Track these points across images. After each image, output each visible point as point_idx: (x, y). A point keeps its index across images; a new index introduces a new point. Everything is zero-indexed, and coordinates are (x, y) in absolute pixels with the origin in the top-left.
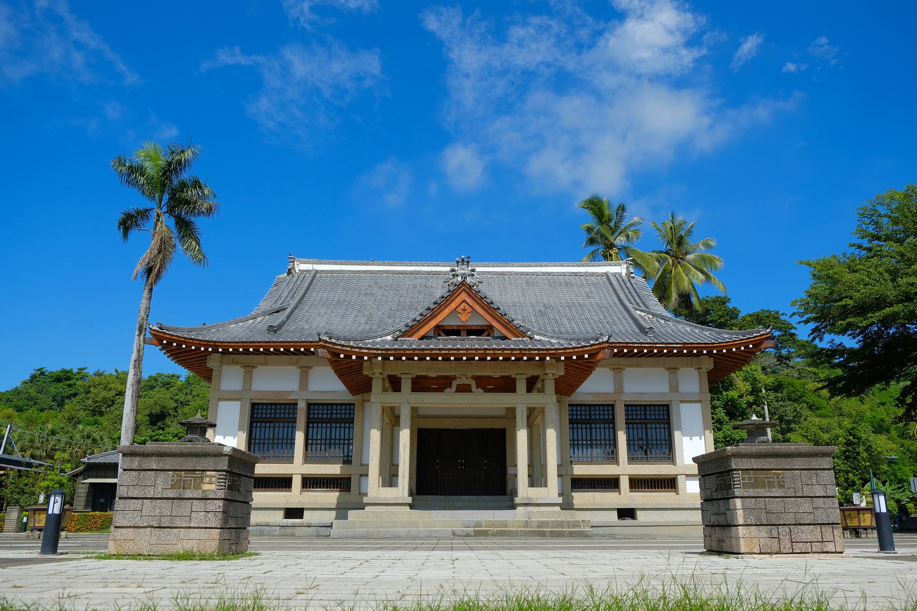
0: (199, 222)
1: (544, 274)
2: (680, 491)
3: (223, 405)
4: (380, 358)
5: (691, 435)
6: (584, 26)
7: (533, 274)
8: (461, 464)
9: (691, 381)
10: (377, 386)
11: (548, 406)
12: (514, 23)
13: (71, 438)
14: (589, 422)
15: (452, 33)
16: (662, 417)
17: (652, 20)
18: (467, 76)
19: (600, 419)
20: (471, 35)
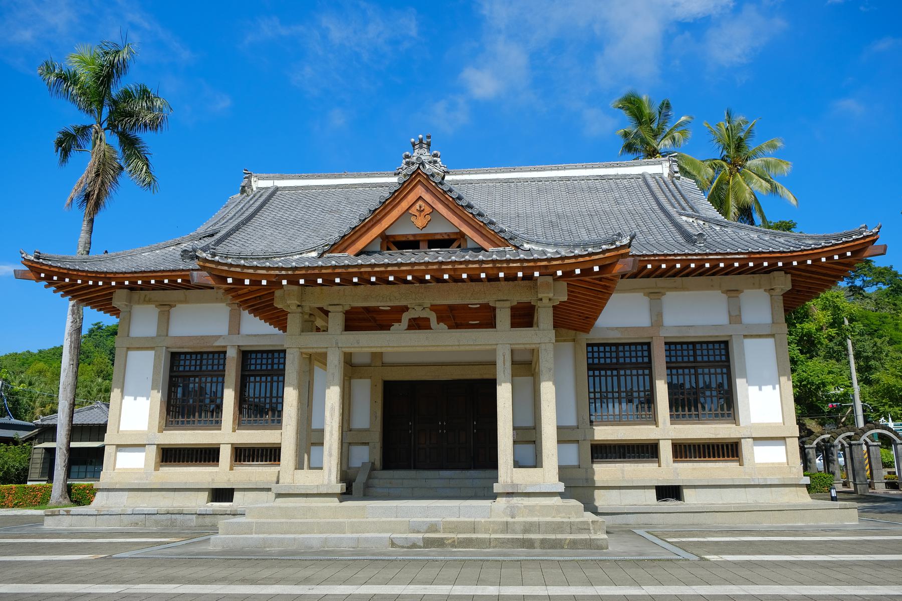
0: (145, 137)
1: (561, 179)
2: (746, 461)
3: (133, 355)
5: (760, 384)
7: (547, 179)
8: (442, 423)
9: (759, 306)
11: (543, 346)
13: (89, 392)
14: (615, 367)
16: (718, 358)
19: (631, 363)
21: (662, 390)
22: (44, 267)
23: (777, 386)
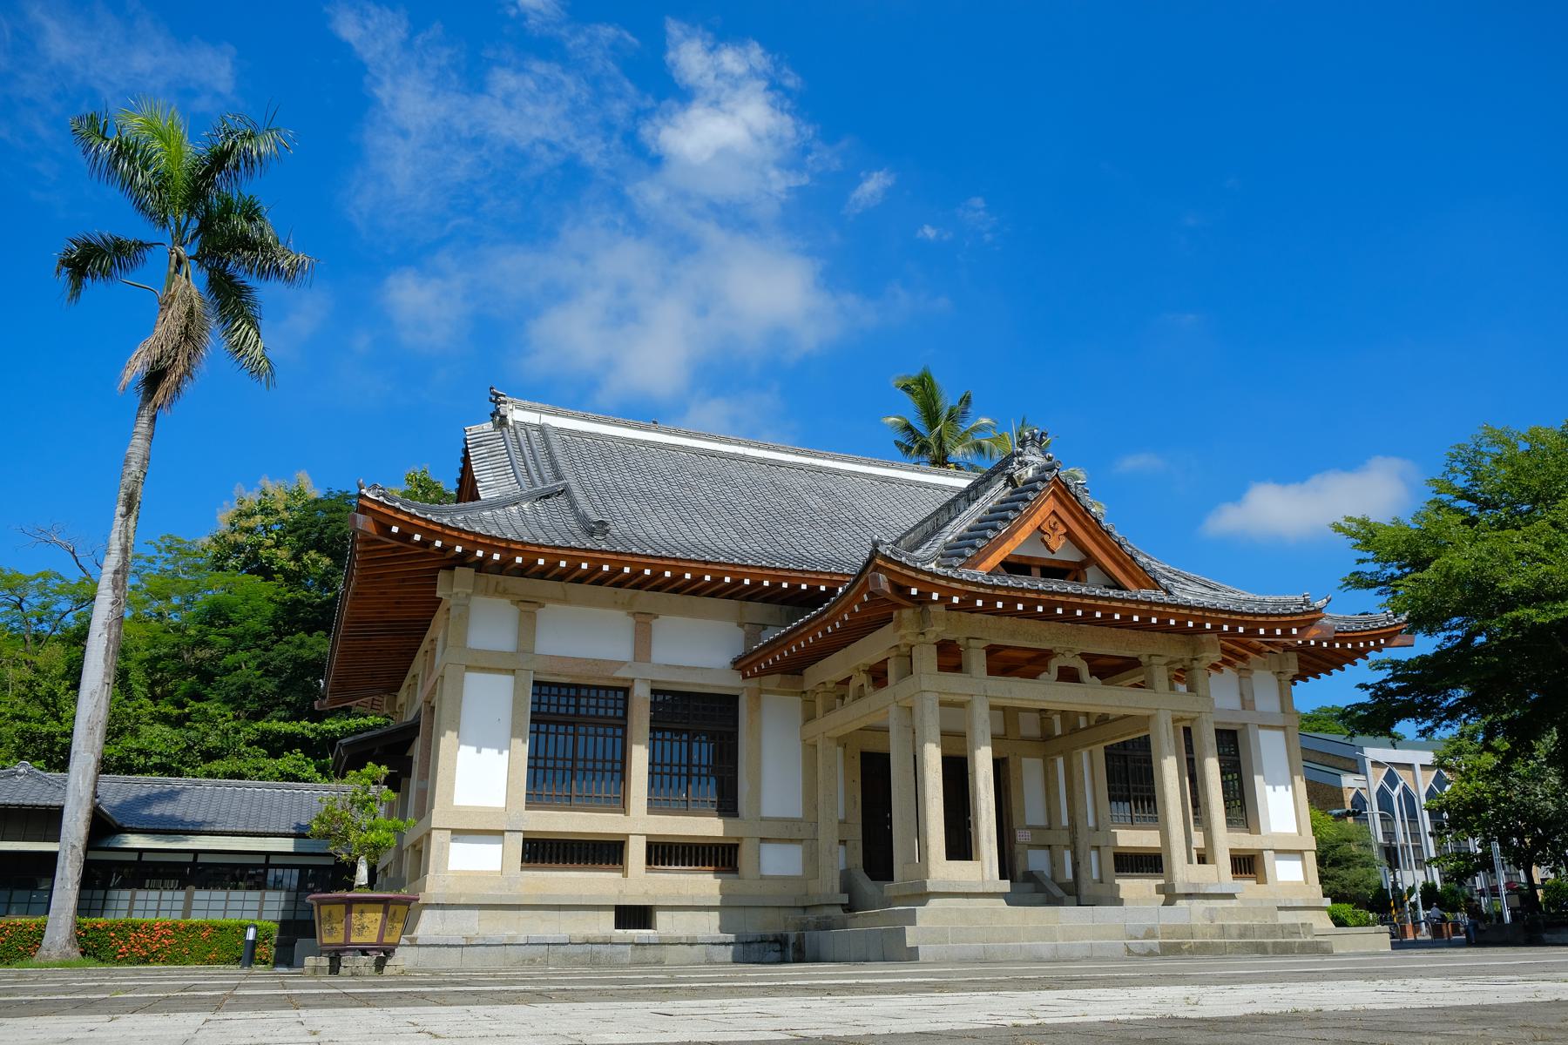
0: (266, 292)
5: (1274, 785)
6: (620, 97)
12: (504, 65)
15: (384, 54)
17: (732, 113)
18: (404, 134)
20: (422, 65)
21: (640, 758)
22: (400, 516)
23: (506, 753)
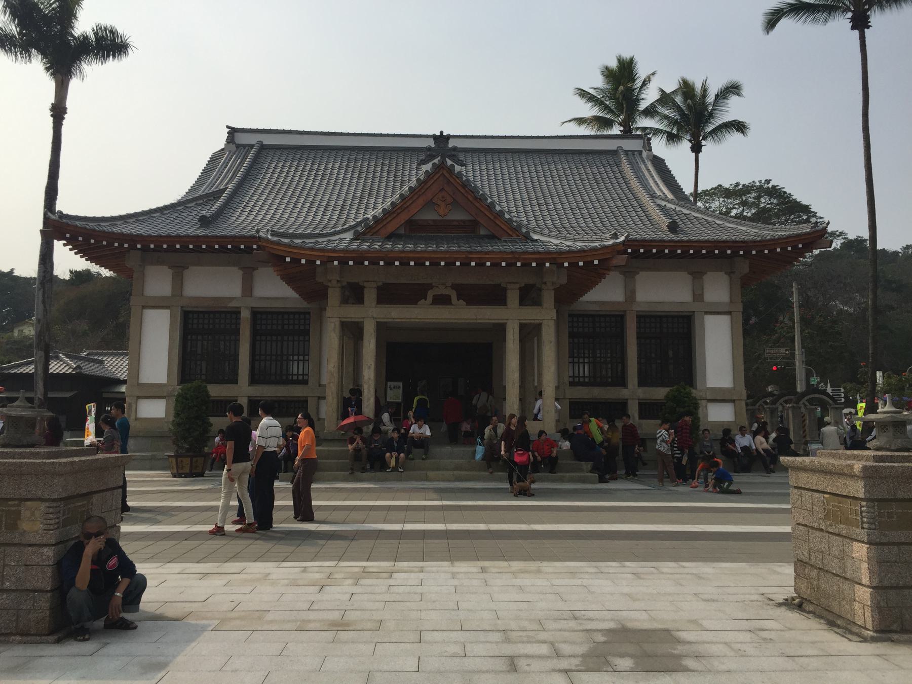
4: (336, 263)
9: (718, 289)
10: (334, 296)
